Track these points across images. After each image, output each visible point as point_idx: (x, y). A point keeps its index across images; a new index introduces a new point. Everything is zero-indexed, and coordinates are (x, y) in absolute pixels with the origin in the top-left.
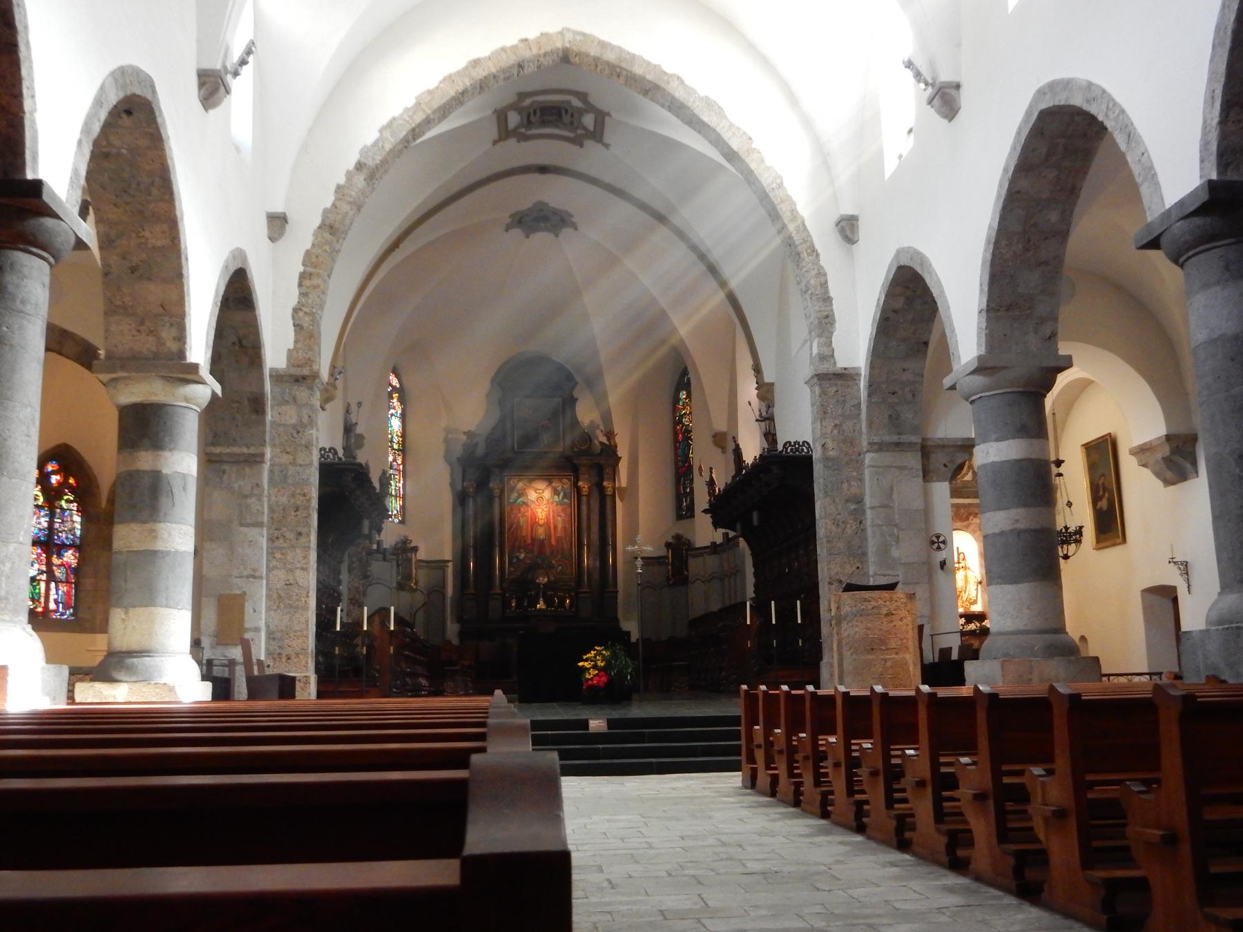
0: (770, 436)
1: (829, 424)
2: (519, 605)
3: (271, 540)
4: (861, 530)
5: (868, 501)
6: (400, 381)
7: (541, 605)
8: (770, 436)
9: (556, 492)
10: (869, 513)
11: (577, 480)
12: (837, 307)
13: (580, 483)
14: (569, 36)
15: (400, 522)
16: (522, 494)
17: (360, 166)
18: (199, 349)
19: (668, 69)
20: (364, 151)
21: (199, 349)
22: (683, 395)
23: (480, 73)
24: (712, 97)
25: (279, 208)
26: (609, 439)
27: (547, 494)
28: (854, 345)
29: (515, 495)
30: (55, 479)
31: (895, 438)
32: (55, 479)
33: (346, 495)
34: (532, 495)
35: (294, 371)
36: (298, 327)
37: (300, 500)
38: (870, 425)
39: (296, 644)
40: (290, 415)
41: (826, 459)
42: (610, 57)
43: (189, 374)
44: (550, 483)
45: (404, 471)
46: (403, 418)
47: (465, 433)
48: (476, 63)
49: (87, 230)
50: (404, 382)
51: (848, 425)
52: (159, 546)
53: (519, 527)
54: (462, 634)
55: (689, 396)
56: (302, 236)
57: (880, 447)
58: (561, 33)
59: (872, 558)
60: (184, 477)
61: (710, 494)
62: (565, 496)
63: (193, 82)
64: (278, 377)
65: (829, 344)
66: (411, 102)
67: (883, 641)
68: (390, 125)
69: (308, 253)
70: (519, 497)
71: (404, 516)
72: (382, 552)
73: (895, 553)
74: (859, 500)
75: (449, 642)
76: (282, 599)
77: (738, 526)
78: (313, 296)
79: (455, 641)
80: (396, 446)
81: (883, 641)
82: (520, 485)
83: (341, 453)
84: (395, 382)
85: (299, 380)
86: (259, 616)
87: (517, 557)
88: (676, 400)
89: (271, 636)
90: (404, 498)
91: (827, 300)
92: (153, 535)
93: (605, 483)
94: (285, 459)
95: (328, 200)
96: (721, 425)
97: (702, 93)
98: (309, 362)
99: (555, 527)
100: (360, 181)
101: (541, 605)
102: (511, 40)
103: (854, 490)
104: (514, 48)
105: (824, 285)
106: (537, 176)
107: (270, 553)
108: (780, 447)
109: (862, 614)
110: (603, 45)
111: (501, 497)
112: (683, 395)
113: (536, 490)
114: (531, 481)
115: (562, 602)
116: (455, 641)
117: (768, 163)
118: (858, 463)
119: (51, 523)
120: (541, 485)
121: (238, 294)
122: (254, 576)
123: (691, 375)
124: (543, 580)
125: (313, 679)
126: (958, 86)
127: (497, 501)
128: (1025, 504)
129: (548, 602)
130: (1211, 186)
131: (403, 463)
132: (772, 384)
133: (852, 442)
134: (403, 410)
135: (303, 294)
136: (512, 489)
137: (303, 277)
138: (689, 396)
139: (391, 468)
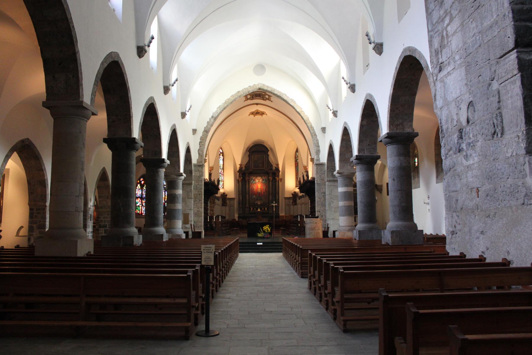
1: (318, 175)
2: (253, 210)
3: (194, 201)
4: (325, 200)
5: (327, 193)
7: (259, 210)
9: (263, 180)
10: (327, 196)
12: (321, 148)
14: (260, 85)
16: (254, 180)
17: (212, 117)
18: (182, 170)
19: (283, 92)
20: (213, 114)
21: (182, 170)
23: (240, 94)
24: (293, 98)
25: (195, 128)
27: (261, 180)
28: (324, 158)
30: (142, 182)
31: (333, 179)
32: (142, 182)
33: (211, 188)
34: (257, 181)
35: (198, 164)
36: (199, 154)
37: (200, 193)
38: (327, 176)
39: (200, 224)
40: (198, 174)
41: (317, 183)
42: (269, 89)
43: (181, 175)
48: (239, 92)
49: (168, 162)
51: (322, 176)
52: (176, 208)
53: (254, 189)
54: (239, 217)
56: (200, 133)
57: (329, 181)
58: (258, 84)
59: (327, 206)
60: (180, 194)
63: (180, 115)
64: (195, 165)
65: (319, 157)
66: (224, 102)
67: (314, 228)
68: (219, 107)
69: (201, 137)
72: (218, 198)
73: (332, 205)
74: (325, 193)
75: (235, 220)
76: (197, 214)
78: (202, 147)
79: (237, 220)
81: (314, 228)
84: (221, 151)
85: (199, 166)
86: (192, 218)
89: (194, 222)
91: (319, 146)
92: (175, 206)
94: (197, 183)
95: (205, 125)
96: (305, 164)
97: (290, 98)
98: (201, 162)
100: (212, 120)
101: (259, 210)
102: (247, 86)
103: (324, 191)
104: (247, 88)
105: (318, 143)
106: (256, 105)
107: (194, 204)
109: (311, 223)
110: (268, 87)
111: (249, 181)
115: (264, 209)
116: (237, 220)
117: (306, 114)
118: (325, 184)
119: (142, 193)
120: (259, 178)
121: (188, 151)
122: (191, 210)
124: (259, 203)
125: (203, 231)
126: (337, 111)
127: (247, 182)
128: (345, 200)
129: (261, 209)
130: (388, 133)
133: (323, 180)
135: (200, 147)
136: (252, 179)
137: (200, 142)
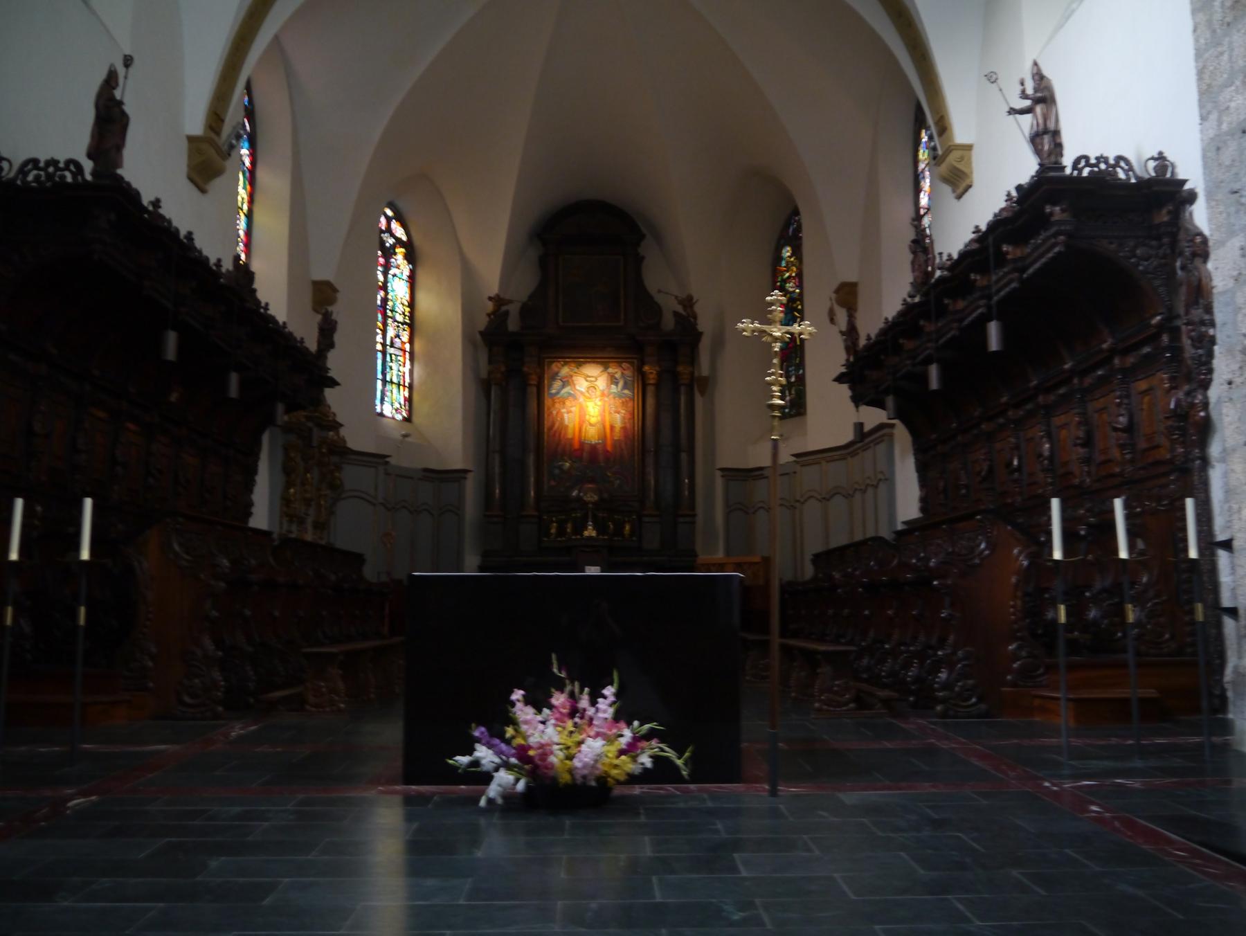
0: (1046, 140)
2: (561, 531)
6: (407, 233)
7: (590, 532)
8: (1046, 140)
11: (643, 363)
13: (646, 368)
15: (405, 419)
22: (787, 252)
26: (685, 307)
27: (602, 383)
29: (557, 384)
44: (606, 368)
45: (412, 354)
46: (412, 279)
47: (490, 299)
50: (413, 234)
55: (797, 252)
61: (848, 349)
62: (625, 387)
70: (563, 386)
71: (410, 411)
77: (890, 401)
80: (400, 318)
82: (565, 371)
83: (88, 166)
84: (399, 232)
87: (560, 468)
88: (778, 258)
90: (411, 387)
93: (680, 369)
99: (612, 428)
101: (590, 532)
108: (1067, 161)
112: (787, 252)
113: (586, 377)
114: (579, 365)
115: (619, 530)
123: (806, 220)
129: (600, 528)
131: (411, 341)
132: (969, 148)
134: (412, 272)
136: (554, 377)
138: (797, 252)
139: (392, 346)
